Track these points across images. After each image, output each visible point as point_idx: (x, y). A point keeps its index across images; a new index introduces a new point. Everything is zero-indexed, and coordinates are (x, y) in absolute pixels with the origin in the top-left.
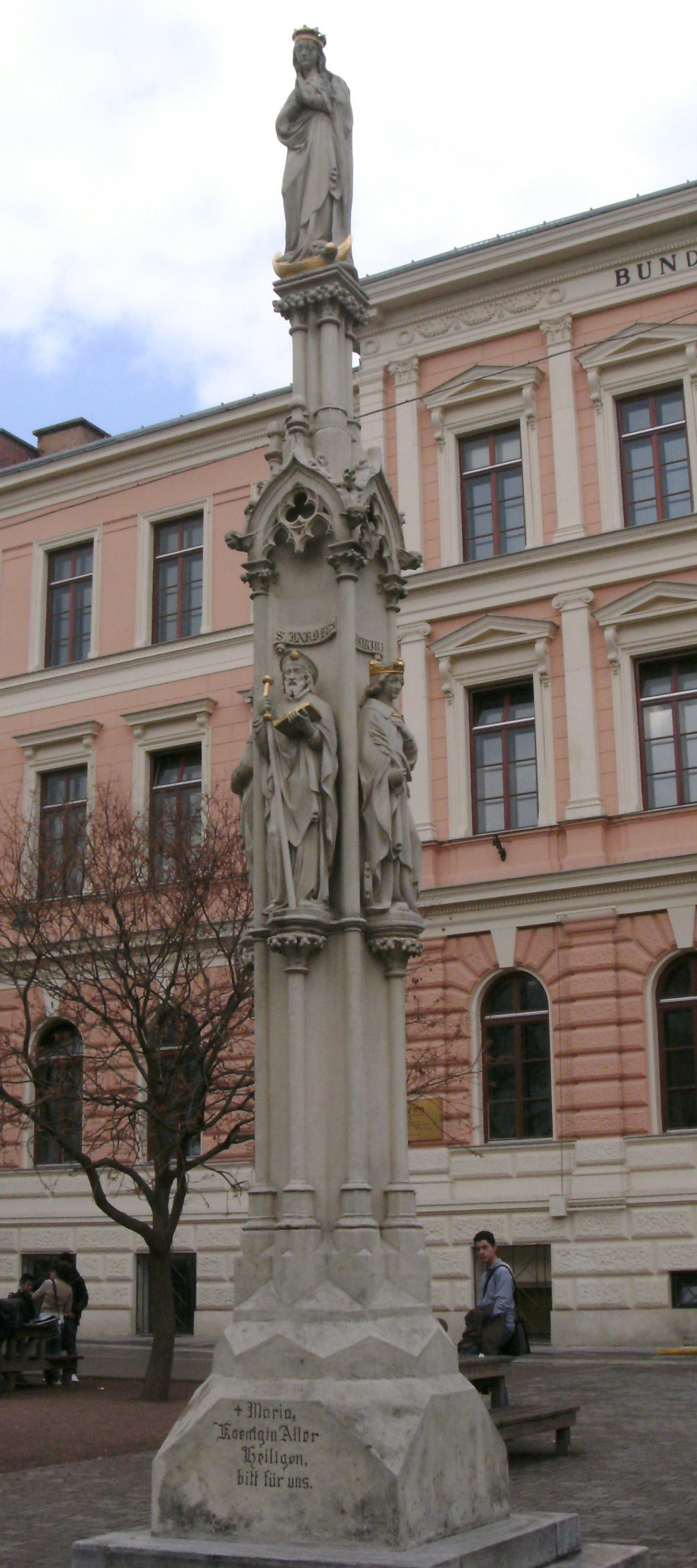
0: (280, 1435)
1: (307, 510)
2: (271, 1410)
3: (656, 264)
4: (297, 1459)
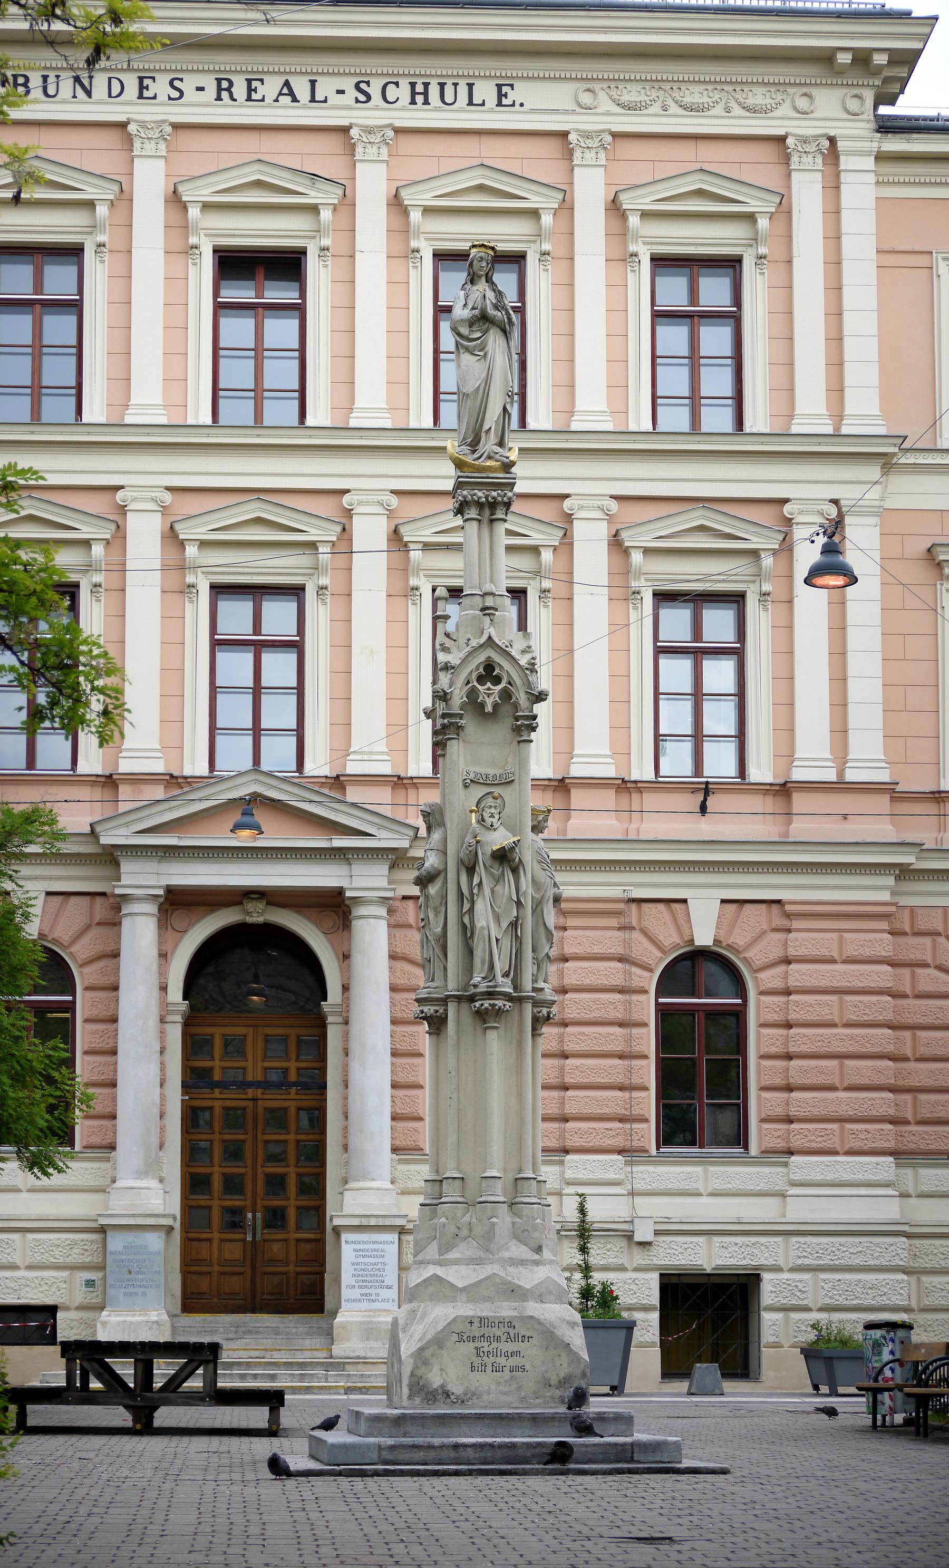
0: (504, 1338)
1: (497, 680)
4: (517, 1353)
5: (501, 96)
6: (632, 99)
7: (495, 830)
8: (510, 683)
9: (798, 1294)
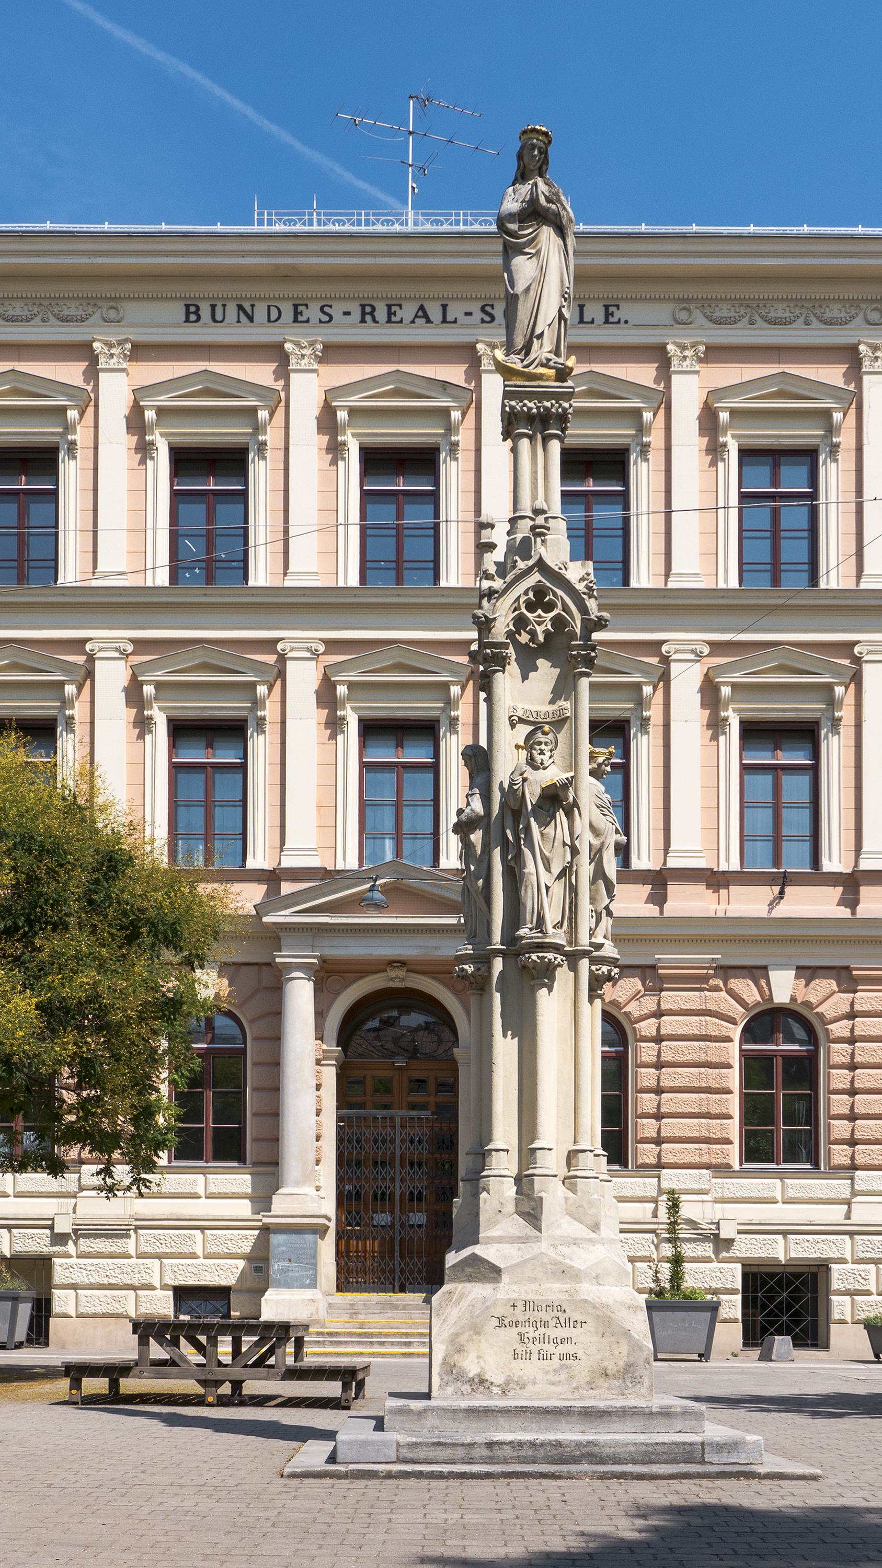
0: (552, 1323)
1: (549, 607)
2: (544, 1306)
3: (232, 311)
4: (569, 1340)
5: (608, 314)
6: (723, 315)
7: (545, 768)
8: (563, 610)
9: (862, 1281)
